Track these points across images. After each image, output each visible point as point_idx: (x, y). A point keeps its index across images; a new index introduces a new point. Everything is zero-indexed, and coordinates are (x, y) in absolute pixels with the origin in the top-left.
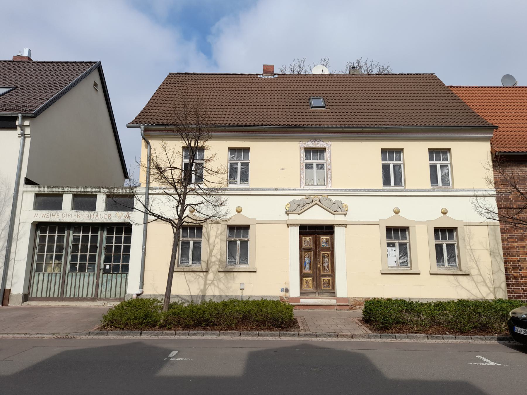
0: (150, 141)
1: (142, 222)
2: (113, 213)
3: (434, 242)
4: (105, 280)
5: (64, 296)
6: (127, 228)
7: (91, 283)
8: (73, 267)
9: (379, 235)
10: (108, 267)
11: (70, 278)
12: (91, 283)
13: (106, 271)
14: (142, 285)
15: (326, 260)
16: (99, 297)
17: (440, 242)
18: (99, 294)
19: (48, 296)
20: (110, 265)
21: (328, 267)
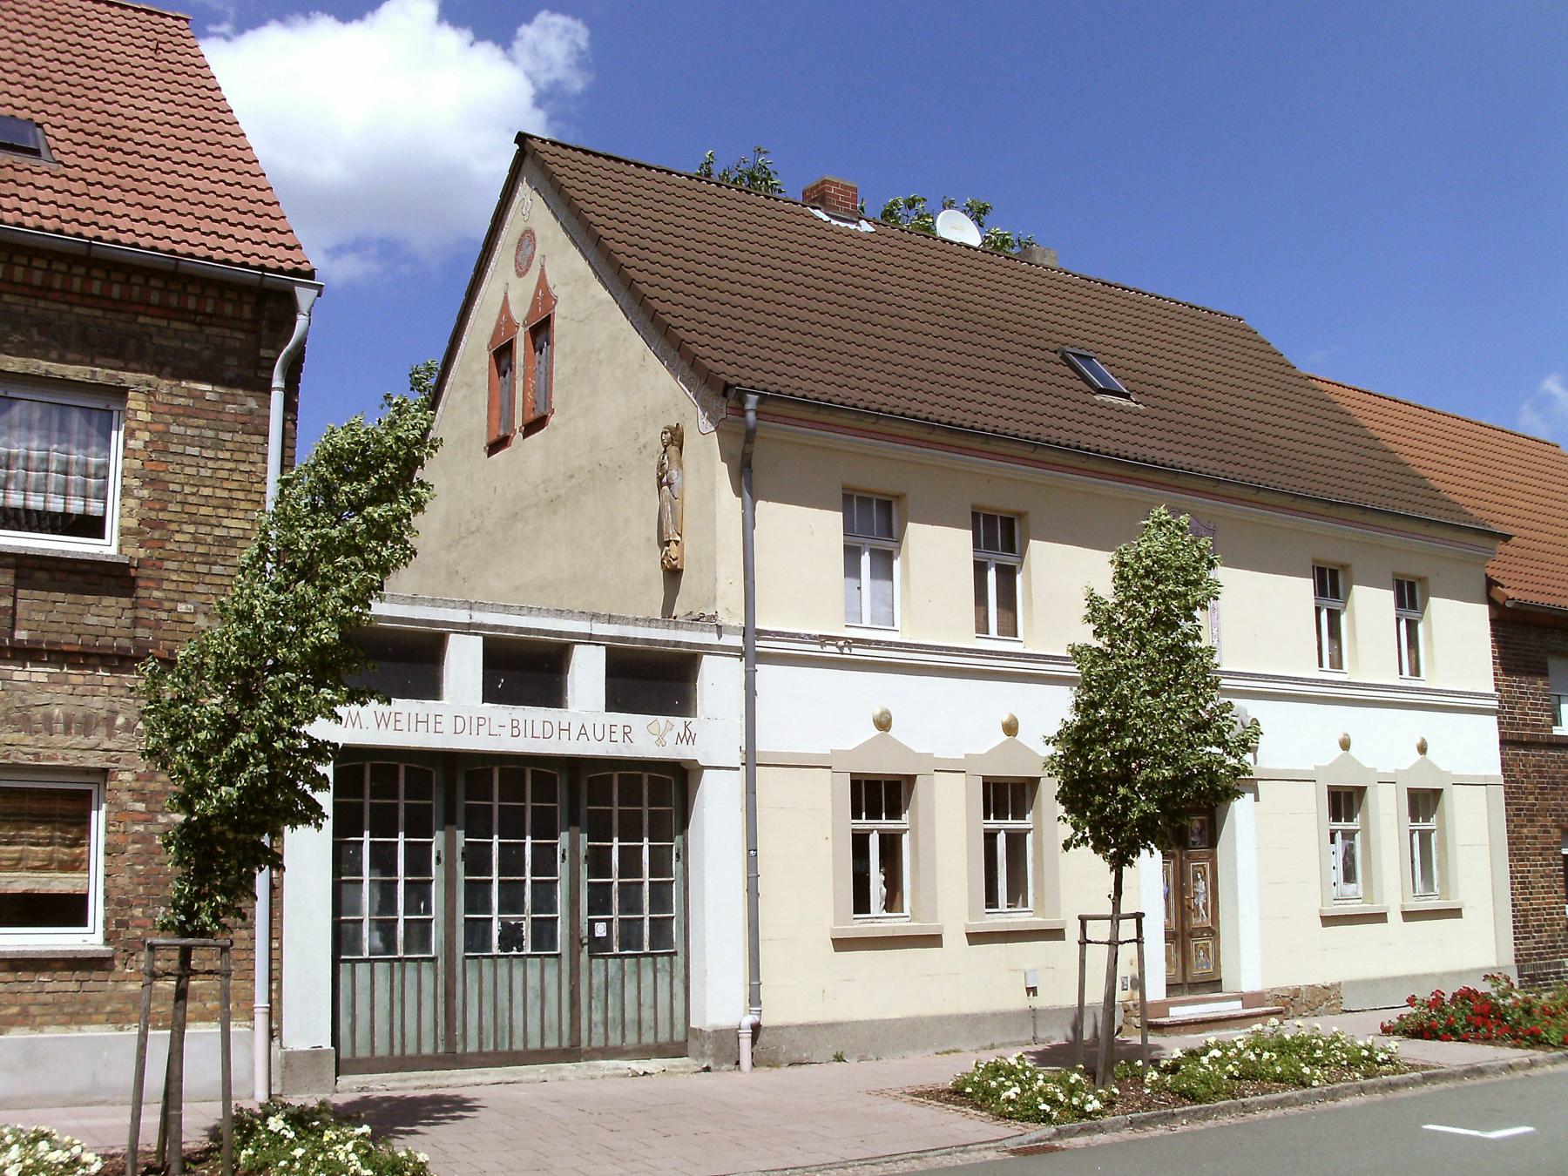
0: (389, 608)
1: (736, 759)
2: (639, 722)
3: (849, 825)
4: (598, 979)
5: (459, 1049)
6: (673, 784)
7: (552, 993)
8: (477, 934)
9: (1314, 803)
10: (601, 930)
11: (472, 976)
12: (552, 993)
13: (599, 947)
14: (754, 999)
15: (1201, 883)
16: (584, 1044)
17: (864, 823)
18: (584, 1034)
19: (397, 1051)
20: (609, 922)
21: (1205, 907)
